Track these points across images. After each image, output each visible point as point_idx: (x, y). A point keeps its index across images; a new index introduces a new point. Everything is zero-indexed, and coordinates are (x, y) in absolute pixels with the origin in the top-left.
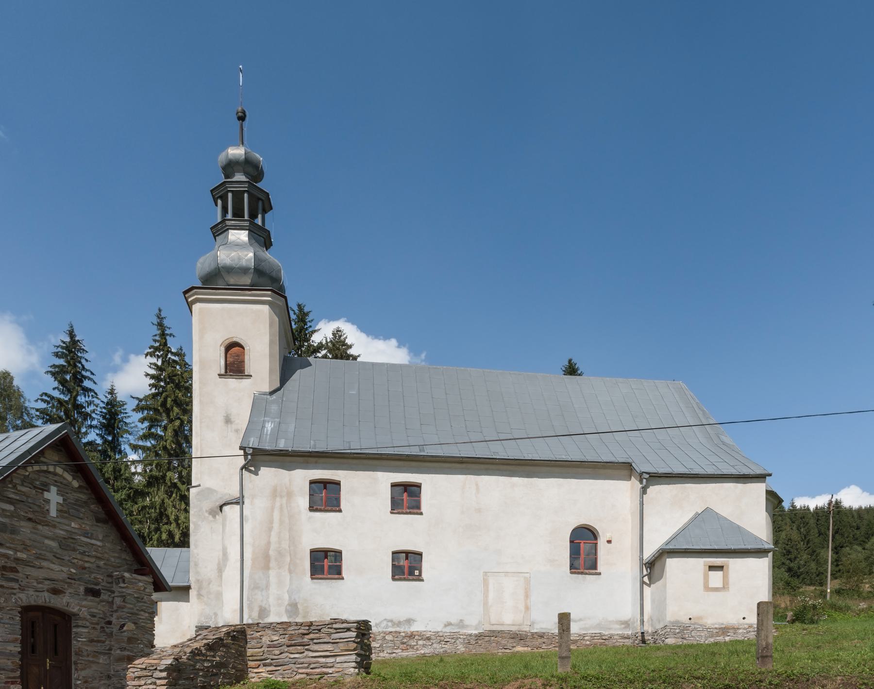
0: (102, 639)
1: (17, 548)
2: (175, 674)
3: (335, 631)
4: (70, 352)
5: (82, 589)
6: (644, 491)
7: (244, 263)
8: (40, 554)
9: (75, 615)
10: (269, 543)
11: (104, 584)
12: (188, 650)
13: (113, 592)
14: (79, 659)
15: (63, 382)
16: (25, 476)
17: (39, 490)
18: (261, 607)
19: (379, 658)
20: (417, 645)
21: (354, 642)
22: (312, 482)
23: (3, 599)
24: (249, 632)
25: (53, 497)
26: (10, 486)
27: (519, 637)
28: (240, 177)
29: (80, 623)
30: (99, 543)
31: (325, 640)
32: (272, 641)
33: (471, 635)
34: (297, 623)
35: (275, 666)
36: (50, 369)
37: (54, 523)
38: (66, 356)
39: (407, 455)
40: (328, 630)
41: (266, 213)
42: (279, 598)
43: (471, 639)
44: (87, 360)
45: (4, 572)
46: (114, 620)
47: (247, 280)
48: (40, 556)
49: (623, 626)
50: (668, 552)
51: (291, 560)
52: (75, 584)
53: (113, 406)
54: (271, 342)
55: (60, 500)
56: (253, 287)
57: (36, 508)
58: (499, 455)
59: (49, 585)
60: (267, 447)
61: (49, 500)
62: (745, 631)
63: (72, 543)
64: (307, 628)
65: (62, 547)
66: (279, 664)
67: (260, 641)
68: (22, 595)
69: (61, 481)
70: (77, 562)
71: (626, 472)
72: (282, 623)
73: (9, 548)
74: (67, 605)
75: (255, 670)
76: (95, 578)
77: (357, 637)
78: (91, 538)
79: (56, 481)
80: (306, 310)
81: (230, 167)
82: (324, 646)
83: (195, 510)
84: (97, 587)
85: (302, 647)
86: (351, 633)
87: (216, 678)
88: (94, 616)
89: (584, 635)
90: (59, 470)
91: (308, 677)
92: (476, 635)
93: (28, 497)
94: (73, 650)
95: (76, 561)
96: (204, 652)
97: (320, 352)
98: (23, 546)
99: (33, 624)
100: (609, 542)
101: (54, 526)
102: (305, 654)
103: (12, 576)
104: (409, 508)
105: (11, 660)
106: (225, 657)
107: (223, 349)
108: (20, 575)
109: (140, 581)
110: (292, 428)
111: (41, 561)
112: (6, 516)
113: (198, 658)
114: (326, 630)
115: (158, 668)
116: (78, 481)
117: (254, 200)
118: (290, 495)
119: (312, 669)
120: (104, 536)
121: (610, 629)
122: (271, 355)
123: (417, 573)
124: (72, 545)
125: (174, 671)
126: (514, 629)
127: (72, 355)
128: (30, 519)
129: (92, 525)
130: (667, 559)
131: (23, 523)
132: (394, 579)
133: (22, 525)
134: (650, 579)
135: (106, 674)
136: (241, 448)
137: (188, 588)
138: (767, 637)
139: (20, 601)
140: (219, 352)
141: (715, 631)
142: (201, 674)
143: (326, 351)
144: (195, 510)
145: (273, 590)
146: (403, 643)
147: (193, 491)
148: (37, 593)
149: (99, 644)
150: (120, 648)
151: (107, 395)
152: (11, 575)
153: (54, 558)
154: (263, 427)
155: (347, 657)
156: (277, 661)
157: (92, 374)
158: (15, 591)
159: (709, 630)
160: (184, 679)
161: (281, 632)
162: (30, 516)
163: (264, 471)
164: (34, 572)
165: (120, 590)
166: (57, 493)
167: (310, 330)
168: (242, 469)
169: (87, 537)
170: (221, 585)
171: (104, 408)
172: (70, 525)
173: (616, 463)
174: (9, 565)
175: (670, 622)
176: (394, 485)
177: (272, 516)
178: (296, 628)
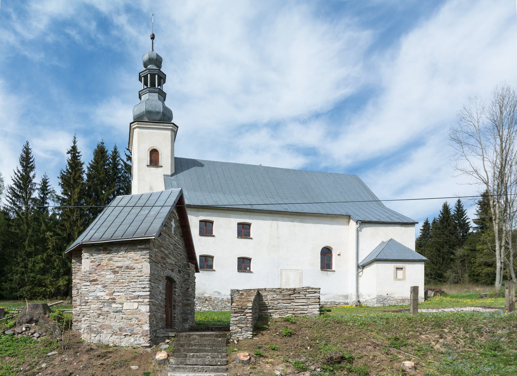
3: (308, 293)
22: (200, 221)
31: (303, 297)
32: (273, 297)
49: (345, 298)
64: (293, 291)
66: (277, 309)
67: (266, 297)
85: (289, 301)
95: (176, 256)
102: (291, 304)
104: (244, 236)
123: (248, 269)
141: (399, 300)
178: (287, 291)
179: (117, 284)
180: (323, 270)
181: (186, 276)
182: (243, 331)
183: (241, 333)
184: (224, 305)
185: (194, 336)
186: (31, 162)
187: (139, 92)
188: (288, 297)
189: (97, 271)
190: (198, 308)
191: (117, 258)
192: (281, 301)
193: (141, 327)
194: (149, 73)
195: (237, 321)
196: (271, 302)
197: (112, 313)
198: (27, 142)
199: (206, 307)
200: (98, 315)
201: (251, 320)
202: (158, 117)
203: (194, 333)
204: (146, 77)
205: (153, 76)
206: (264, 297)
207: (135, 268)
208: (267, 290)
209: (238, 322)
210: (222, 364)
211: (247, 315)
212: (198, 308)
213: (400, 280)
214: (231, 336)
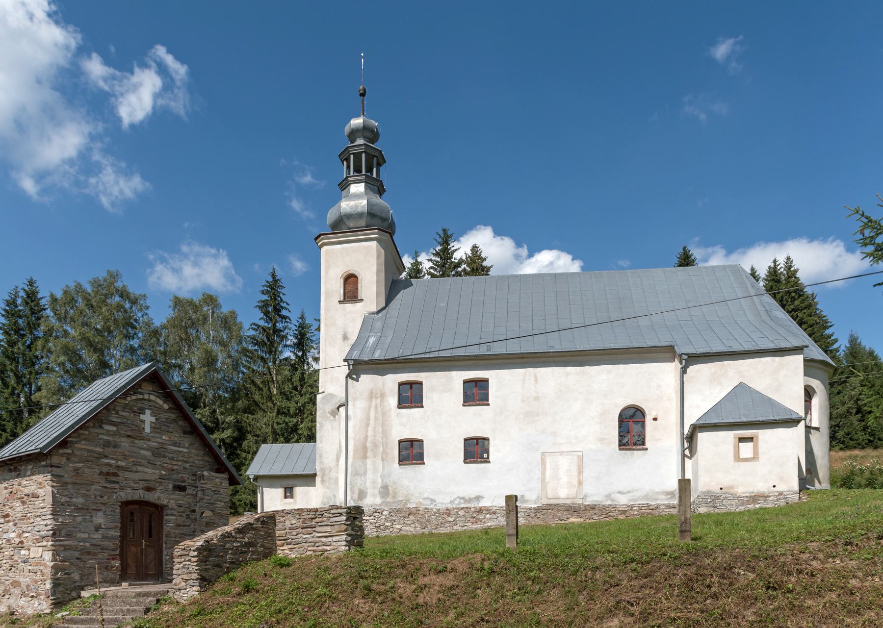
3: (332, 516)
4: (272, 289)
5: (171, 486)
6: (684, 371)
7: (360, 210)
8: (137, 462)
9: (166, 506)
10: (366, 437)
11: (190, 481)
13: (197, 487)
14: (167, 540)
15: (266, 313)
16: (126, 404)
18: (360, 490)
19: (453, 531)
20: (485, 518)
21: (344, 524)
24: (277, 517)
26: (113, 412)
27: (573, 509)
28: (360, 141)
29: (169, 512)
30: (185, 450)
33: (530, 509)
35: (294, 545)
36: (258, 304)
37: (148, 437)
38: (269, 292)
39: (475, 356)
41: (381, 166)
42: (374, 482)
43: (531, 512)
44: (283, 294)
45: (107, 477)
46: (197, 508)
47: (363, 223)
49: (669, 496)
50: (699, 427)
51: (383, 450)
53: (303, 328)
54: (378, 271)
55: (153, 419)
56: (368, 227)
57: (134, 427)
58: (554, 349)
62: (775, 499)
63: (163, 451)
64: (314, 513)
68: (121, 493)
71: (669, 355)
72: (298, 509)
73: (112, 459)
75: (281, 548)
76: (181, 477)
77: (347, 520)
78: (179, 447)
79: (150, 406)
80: (449, 233)
81: (354, 134)
83: (320, 412)
84: (183, 484)
85: (311, 529)
86: (343, 517)
87: (245, 555)
88: (181, 507)
89: (632, 506)
90: (153, 398)
92: (535, 509)
93: (128, 419)
95: (166, 465)
96: (234, 534)
97: (460, 267)
98: (123, 457)
100: (655, 419)
101: (149, 440)
102: (312, 535)
103: (113, 480)
106: (253, 538)
107: (342, 280)
108: (120, 478)
109: (217, 477)
111: (138, 467)
112: (110, 435)
113: (227, 539)
115: (192, 549)
116: (168, 405)
117: (370, 158)
118: (383, 396)
119: (317, 547)
121: (657, 499)
122: (378, 281)
123: (485, 456)
124: (163, 453)
125: (205, 550)
126: (568, 502)
127: (273, 291)
128: (129, 436)
129: (180, 437)
130: (699, 434)
131: (123, 439)
132: (465, 462)
134: (691, 452)
136: (345, 361)
137: (314, 475)
138: (685, 512)
141: (745, 499)
142: (230, 552)
143: (465, 265)
144: (320, 412)
145: (370, 476)
146: (473, 517)
147: (319, 397)
148: (134, 491)
149: (185, 528)
151: (299, 320)
152: (114, 479)
154: (367, 341)
155: (340, 537)
157: (288, 304)
158: (115, 490)
159: (740, 499)
161: (297, 517)
162: (129, 433)
163: (364, 378)
167: (453, 249)
168: (347, 377)
169: (176, 446)
170: (337, 473)
171: (296, 330)
172: (162, 438)
173: (660, 347)
174: (111, 471)
175: (702, 492)
176: (466, 382)
177: (369, 414)
180: (623, 449)
184: (440, 520)
190: (397, 526)
197: (21, 564)
199: (410, 525)
212: (397, 526)
213: (746, 460)
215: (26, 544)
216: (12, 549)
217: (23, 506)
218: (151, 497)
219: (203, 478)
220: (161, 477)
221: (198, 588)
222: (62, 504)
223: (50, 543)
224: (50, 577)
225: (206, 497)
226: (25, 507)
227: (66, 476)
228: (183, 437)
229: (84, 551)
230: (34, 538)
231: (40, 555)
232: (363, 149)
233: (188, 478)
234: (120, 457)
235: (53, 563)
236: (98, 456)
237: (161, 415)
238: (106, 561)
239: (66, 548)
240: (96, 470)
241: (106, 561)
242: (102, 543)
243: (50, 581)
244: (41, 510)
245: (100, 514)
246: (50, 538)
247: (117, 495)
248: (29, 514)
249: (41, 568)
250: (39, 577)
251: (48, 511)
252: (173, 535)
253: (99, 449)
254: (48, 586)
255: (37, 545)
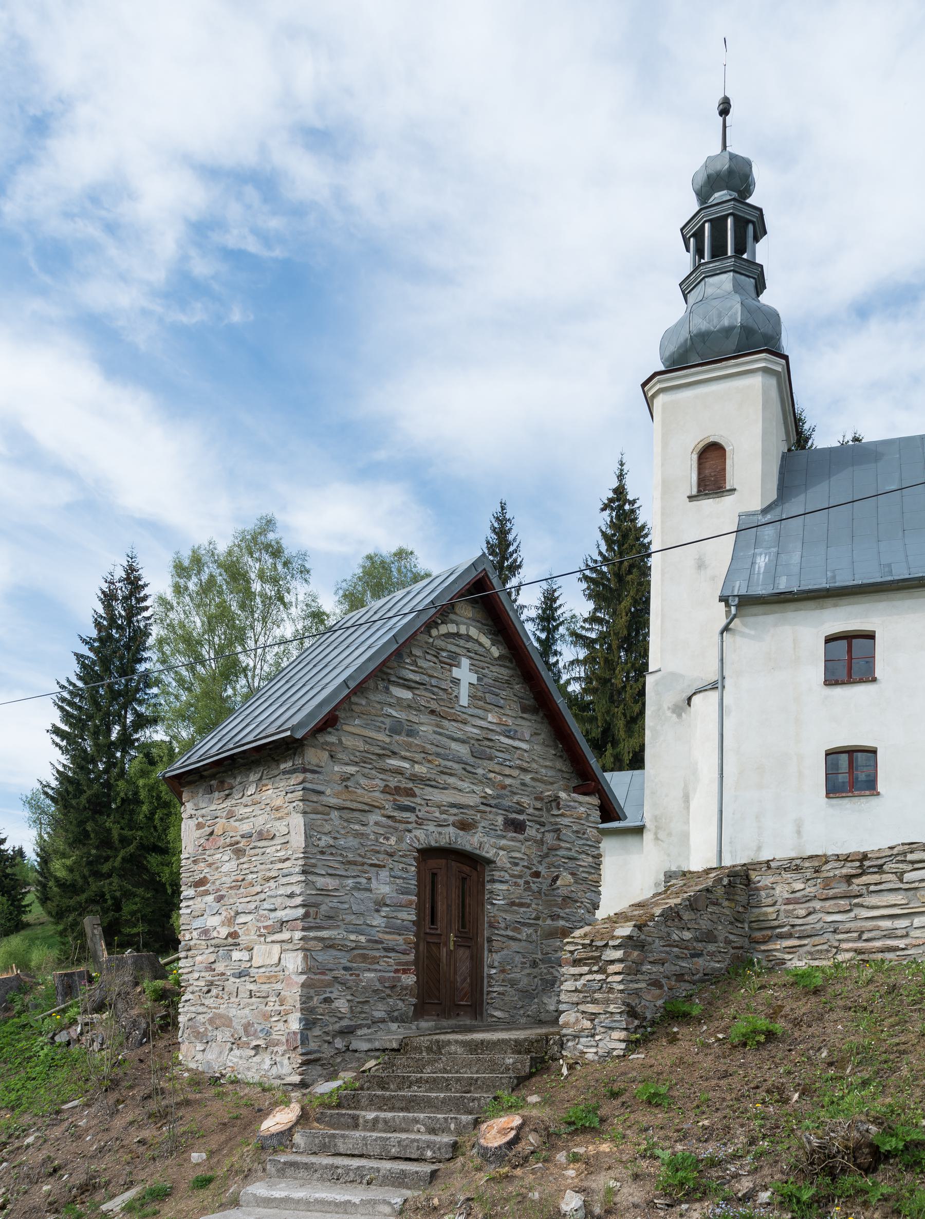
0: (526, 901)
1: (415, 757)
2: (636, 953)
3: (910, 867)
5: (500, 820)
9: (489, 862)
11: (531, 811)
12: (658, 911)
17: (446, 666)
22: (829, 640)
23: (395, 839)
25: (465, 673)
26: (408, 661)
32: (793, 892)
34: (838, 855)
35: (799, 938)
40: (897, 866)
45: (398, 798)
48: (445, 770)
52: (490, 812)
59: (455, 815)
60: (760, 590)
61: (459, 680)
63: (489, 747)
64: (858, 864)
65: (475, 754)
66: (805, 934)
67: (772, 892)
68: (418, 833)
69: (476, 648)
70: (495, 777)
73: (404, 758)
74: (480, 847)
82: (888, 898)
84: (521, 817)
85: (847, 902)
88: (516, 864)
90: (473, 632)
91: (859, 957)
94: (486, 918)
95: (492, 775)
98: (423, 755)
99: (434, 875)
102: (852, 915)
103: (406, 803)
105: (403, 935)
107: (695, 457)
110: (795, 558)
114: (893, 866)
115: (611, 943)
117: (741, 224)
119: (866, 940)
120: (531, 735)
125: (635, 947)
128: (433, 712)
131: (424, 718)
133: (422, 721)
135: (531, 958)
139: (416, 841)
140: (689, 462)
147: (650, 680)
148: (440, 829)
150: (551, 916)
152: (406, 801)
153: (464, 772)
154: (753, 563)
156: (803, 928)
158: (410, 826)
160: (650, 962)
162: (433, 705)
164: (437, 796)
165: (553, 820)
166: (470, 669)
168: (722, 633)
170: (687, 822)
174: (403, 785)
178: (837, 864)
179: (242, 890)
181: (550, 838)
182: (599, 1029)
183: (593, 1036)
185: (453, 1048)
186: (511, 555)
187: (680, 285)
188: (842, 888)
189: (207, 852)
191: (243, 811)
192: (817, 905)
193: (286, 1021)
194: (706, 221)
195: (580, 992)
196: (786, 911)
197: (232, 979)
198: (501, 503)
200: (208, 986)
201: (621, 987)
202: (732, 344)
203: (451, 1037)
204: (698, 235)
205: (718, 225)
206: (763, 893)
207: (275, 835)
208: (773, 864)
209: (581, 995)
210: (438, 1155)
211: (612, 969)
214: (562, 1046)
215: (243, 940)
216: (211, 949)
217: (238, 859)
218: (470, 842)
219: (558, 804)
220: (485, 801)
221: (622, 1035)
222: (322, 853)
223: (298, 935)
224: (298, 1006)
225: (563, 845)
226: (242, 861)
227: (328, 792)
228: (521, 717)
229: (356, 952)
230: (260, 924)
231: (276, 960)
232: (729, 209)
233: (529, 804)
234: (418, 757)
235: (304, 977)
236: (381, 752)
237: (486, 671)
238: (392, 974)
239: (329, 944)
240: (377, 782)
241: (392, 974)
242: (387, 937)
243: (299, 1015)
244: (280, 866)
245: (384, 874)
246: (300, 924)
247: (412, 835)
248: (250, 876)
249: (278, 986)
250: (273, 1005)
251: (294, 866)
252: (503, 925)
253: (382, 737)
254: (295, 1025)
255: (269, 940)
